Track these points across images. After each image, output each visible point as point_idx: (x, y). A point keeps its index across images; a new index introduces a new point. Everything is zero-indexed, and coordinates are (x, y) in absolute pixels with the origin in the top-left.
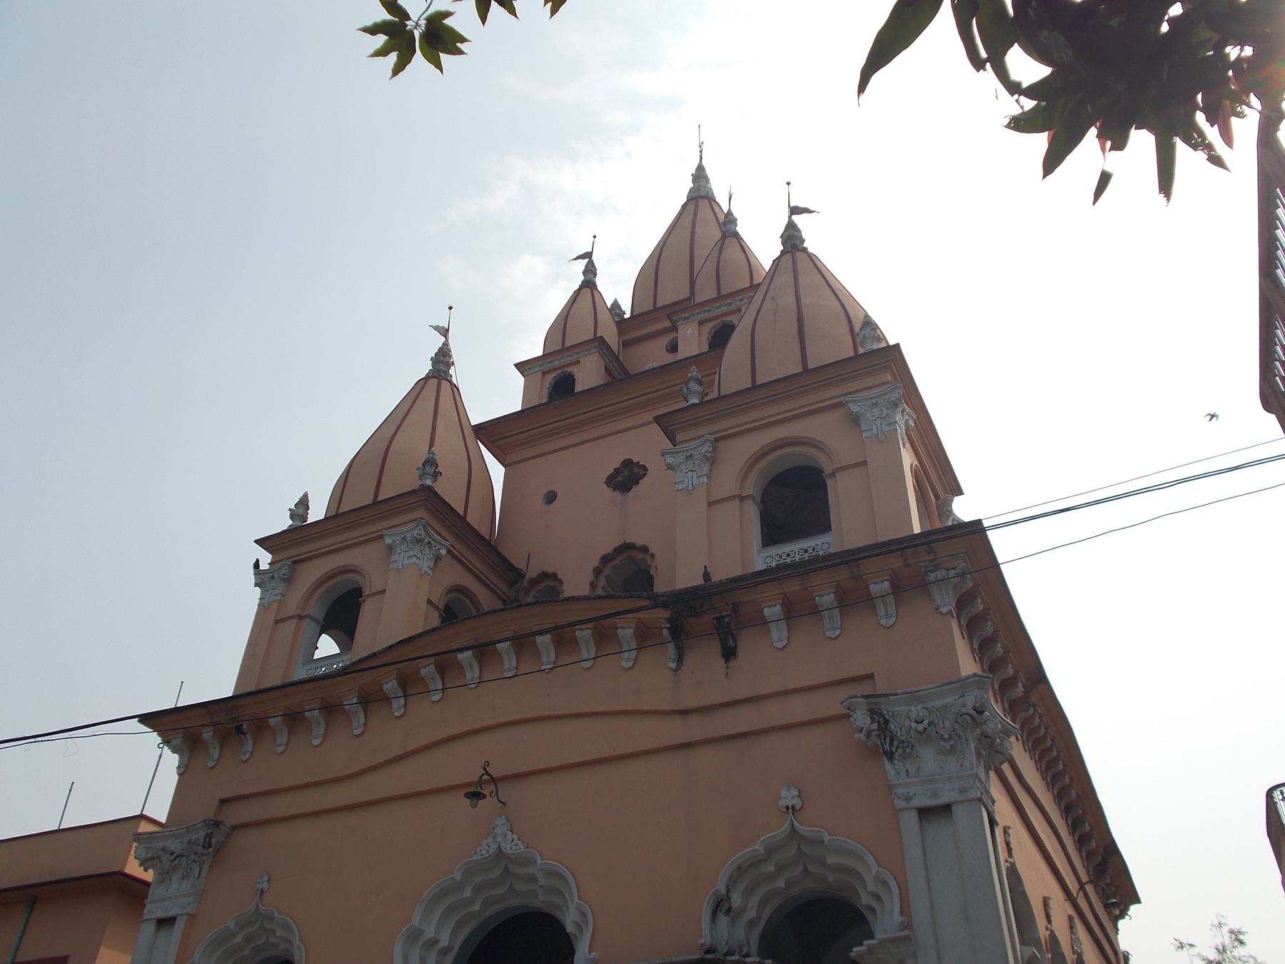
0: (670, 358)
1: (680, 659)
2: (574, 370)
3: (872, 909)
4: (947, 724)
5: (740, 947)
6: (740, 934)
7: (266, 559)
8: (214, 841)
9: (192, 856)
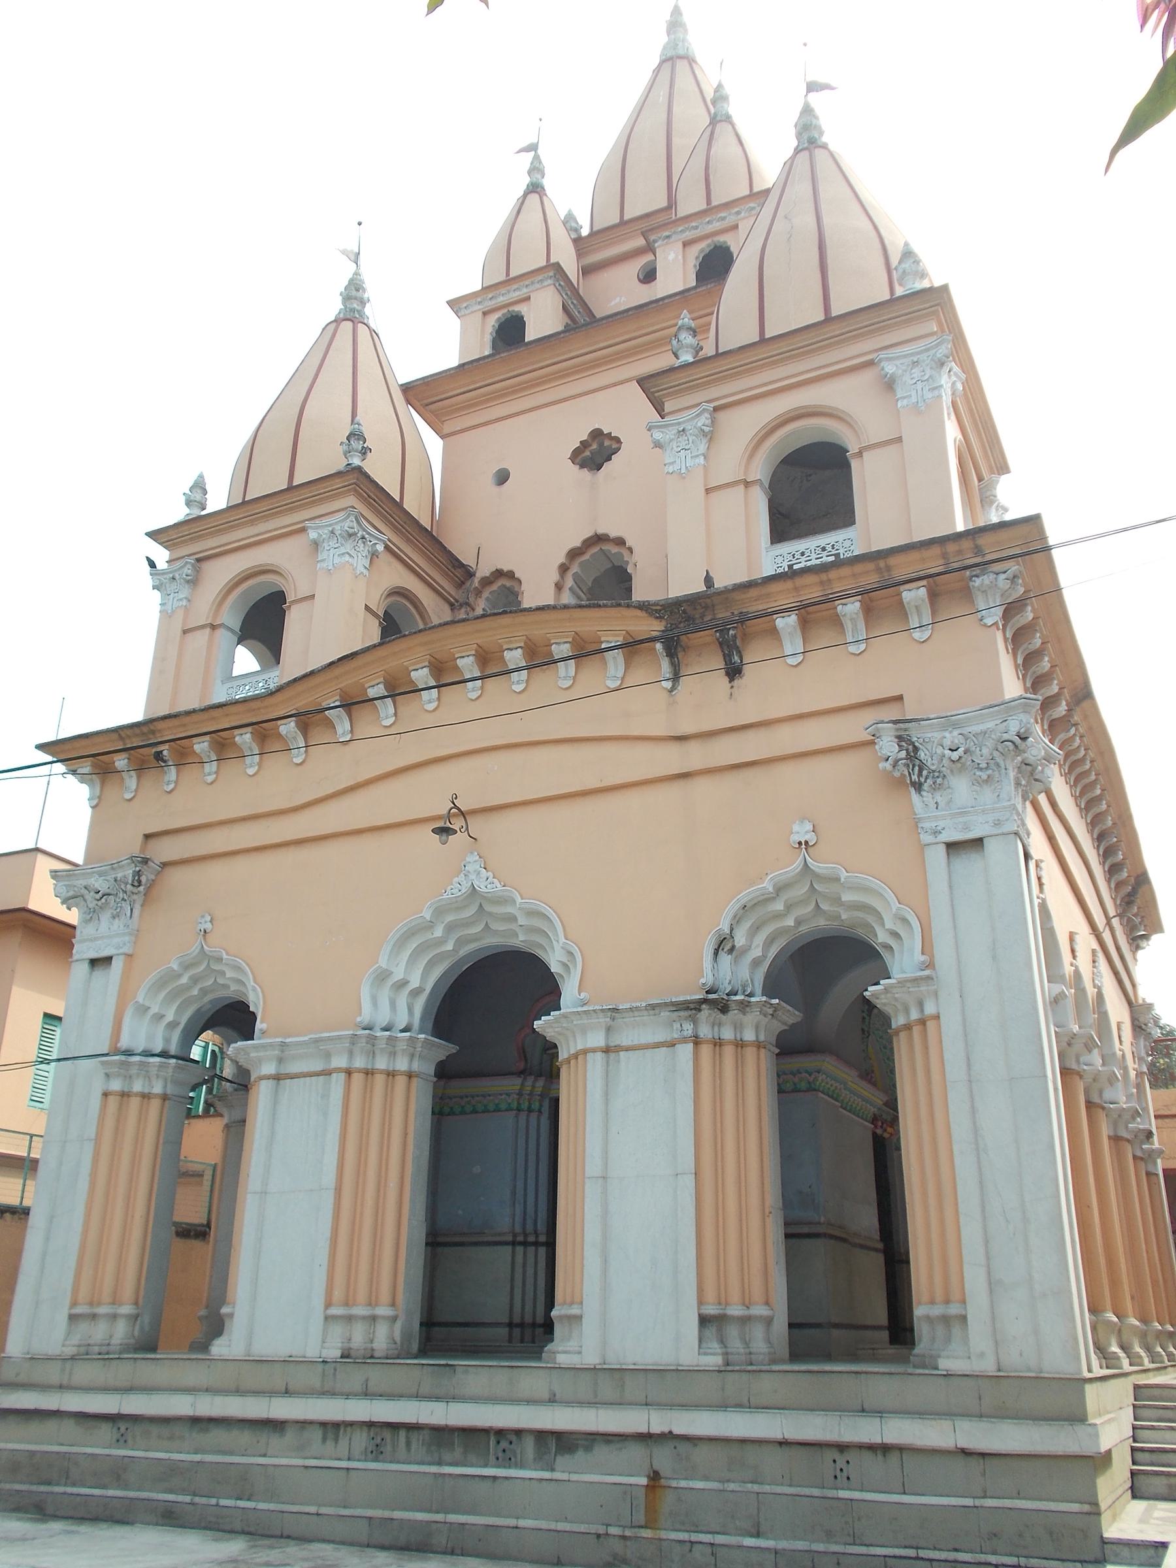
0: (645, 294)
1: (676, 677)
2: (523, 309)
3: (889, 948)
4: (985, 751)
5: (744, 987)
6: (744, 973)
7: (162, 556)
8: (143, 879)
9: (121, 895)
